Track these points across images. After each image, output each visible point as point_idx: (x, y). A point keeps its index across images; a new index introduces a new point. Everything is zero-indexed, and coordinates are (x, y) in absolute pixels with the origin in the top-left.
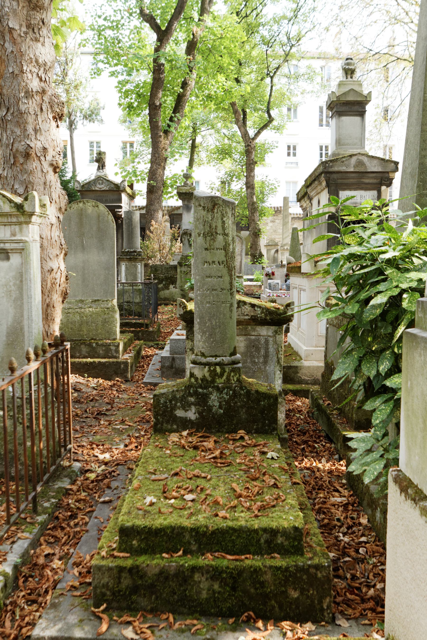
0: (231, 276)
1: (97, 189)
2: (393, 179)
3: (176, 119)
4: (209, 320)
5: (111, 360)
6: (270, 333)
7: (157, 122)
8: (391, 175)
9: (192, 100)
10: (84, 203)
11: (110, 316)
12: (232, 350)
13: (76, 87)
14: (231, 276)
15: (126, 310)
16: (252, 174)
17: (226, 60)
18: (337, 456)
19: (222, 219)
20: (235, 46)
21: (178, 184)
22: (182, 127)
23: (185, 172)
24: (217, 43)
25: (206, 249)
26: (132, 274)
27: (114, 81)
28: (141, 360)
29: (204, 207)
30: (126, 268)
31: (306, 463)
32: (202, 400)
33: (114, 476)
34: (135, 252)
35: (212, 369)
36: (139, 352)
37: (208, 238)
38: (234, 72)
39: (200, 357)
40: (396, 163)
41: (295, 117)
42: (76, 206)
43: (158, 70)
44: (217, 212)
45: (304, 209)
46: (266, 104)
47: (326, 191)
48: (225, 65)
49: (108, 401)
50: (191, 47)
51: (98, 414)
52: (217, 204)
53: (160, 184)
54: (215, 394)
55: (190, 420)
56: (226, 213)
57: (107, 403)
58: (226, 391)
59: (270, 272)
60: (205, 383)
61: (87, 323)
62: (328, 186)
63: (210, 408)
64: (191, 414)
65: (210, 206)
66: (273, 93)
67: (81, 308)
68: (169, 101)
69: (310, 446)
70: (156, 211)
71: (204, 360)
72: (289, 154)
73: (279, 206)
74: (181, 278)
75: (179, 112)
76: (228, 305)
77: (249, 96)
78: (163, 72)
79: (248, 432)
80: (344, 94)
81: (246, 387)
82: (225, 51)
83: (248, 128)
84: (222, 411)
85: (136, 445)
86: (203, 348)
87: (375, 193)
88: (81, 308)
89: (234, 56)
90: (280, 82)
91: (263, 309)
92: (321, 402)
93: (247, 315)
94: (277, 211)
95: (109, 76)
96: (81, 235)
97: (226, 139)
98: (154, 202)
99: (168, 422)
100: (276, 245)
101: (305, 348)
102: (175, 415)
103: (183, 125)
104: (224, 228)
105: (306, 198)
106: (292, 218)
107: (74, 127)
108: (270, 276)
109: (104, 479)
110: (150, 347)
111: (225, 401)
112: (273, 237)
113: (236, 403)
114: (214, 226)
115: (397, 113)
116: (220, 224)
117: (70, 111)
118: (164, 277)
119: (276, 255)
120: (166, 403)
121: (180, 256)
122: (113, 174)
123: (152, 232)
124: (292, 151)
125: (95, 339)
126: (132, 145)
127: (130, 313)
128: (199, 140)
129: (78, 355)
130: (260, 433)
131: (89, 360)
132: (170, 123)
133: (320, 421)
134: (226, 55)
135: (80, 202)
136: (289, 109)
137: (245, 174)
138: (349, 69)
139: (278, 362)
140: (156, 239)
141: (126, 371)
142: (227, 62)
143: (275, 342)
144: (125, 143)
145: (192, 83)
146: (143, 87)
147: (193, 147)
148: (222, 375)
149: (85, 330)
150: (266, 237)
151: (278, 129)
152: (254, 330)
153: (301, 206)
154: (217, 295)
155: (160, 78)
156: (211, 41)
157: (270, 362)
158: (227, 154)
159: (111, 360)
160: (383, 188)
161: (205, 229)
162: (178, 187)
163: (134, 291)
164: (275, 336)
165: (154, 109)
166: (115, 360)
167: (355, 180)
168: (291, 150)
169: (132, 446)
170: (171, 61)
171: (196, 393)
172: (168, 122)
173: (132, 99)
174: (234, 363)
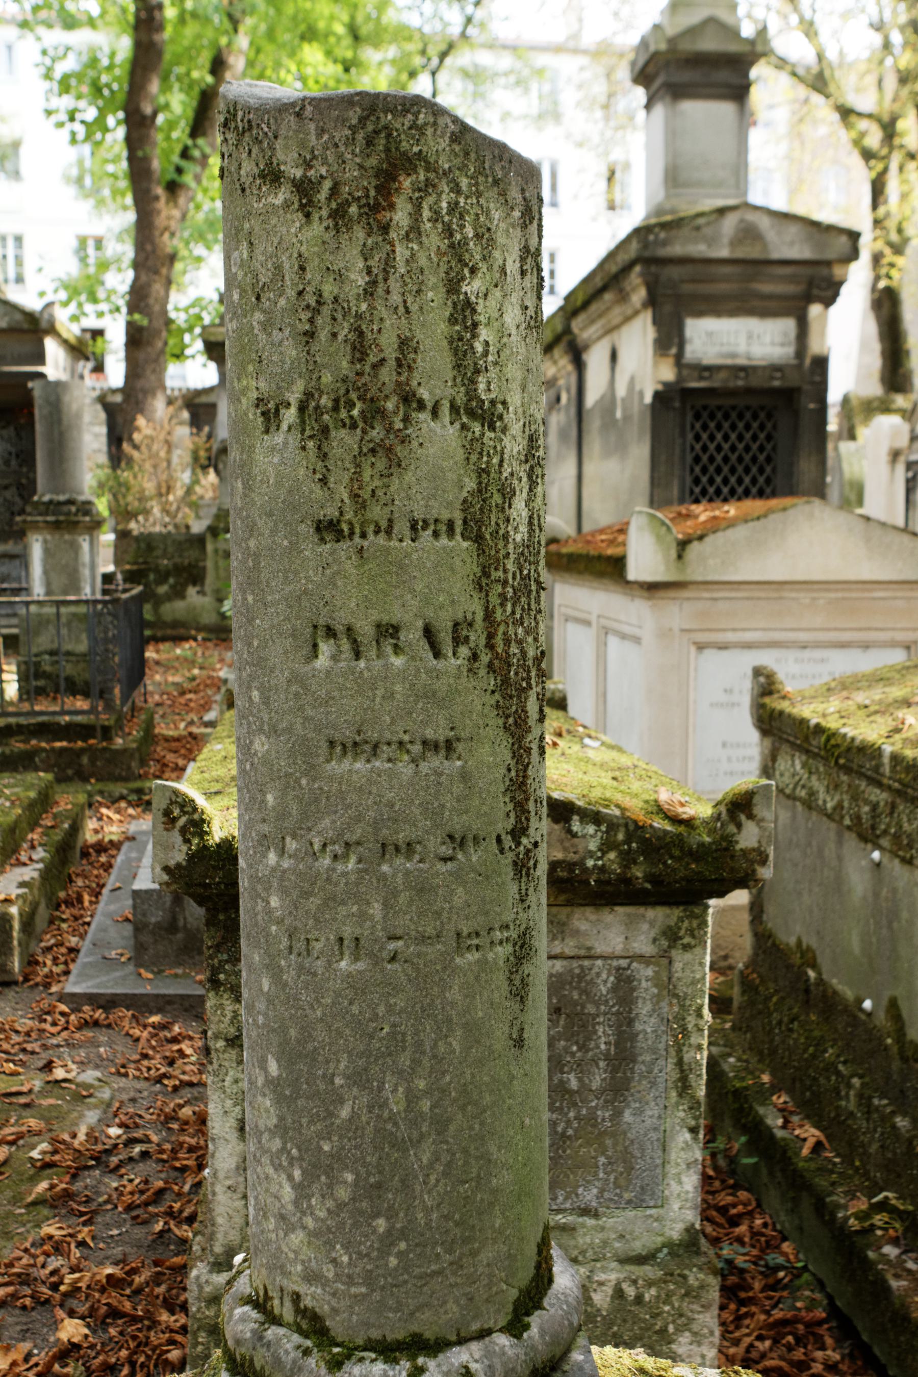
2: (840, 284)
3: (196, 153)
4: (358, 1078)
6: (643, 944)
7: (146, 160)
8: (837, 271)
19: (453, 286)
21: (207, 320)
25: (329, 529)
26: (65, 571)
30: (48, 552)
34: (71, 502)
37: (344, 442)
40: (854, 236)
44: (414, 232)
47: (647, 317)
52: (408, 163)
53: (158, 323)
56: (485, 236)
62: (652, 301)
65: (355, 175)
70: (150, 392)
74: (217, 567)
75: (204, 134)
76: (504, 951)
78: (160, 28)
86: (311, 1277)
87: (788, 325)
91: (612, 826)
110: (113, 801)
114: (388, 343)
116: (433, 329)
121: (214, 510)
123: (136, 447)
126: (99, 243)
132: (183, 163)
133: (773, 1198)
139: (684, 1086)
140: (148, 466)
143: (667, 987)
144: (82, 242)
145: (237, 63)
154: (422, 889)
157: (639, 1085)
160: (815, 310)
161: (313, 368)
164: (665, 956)
165: (139, 126)
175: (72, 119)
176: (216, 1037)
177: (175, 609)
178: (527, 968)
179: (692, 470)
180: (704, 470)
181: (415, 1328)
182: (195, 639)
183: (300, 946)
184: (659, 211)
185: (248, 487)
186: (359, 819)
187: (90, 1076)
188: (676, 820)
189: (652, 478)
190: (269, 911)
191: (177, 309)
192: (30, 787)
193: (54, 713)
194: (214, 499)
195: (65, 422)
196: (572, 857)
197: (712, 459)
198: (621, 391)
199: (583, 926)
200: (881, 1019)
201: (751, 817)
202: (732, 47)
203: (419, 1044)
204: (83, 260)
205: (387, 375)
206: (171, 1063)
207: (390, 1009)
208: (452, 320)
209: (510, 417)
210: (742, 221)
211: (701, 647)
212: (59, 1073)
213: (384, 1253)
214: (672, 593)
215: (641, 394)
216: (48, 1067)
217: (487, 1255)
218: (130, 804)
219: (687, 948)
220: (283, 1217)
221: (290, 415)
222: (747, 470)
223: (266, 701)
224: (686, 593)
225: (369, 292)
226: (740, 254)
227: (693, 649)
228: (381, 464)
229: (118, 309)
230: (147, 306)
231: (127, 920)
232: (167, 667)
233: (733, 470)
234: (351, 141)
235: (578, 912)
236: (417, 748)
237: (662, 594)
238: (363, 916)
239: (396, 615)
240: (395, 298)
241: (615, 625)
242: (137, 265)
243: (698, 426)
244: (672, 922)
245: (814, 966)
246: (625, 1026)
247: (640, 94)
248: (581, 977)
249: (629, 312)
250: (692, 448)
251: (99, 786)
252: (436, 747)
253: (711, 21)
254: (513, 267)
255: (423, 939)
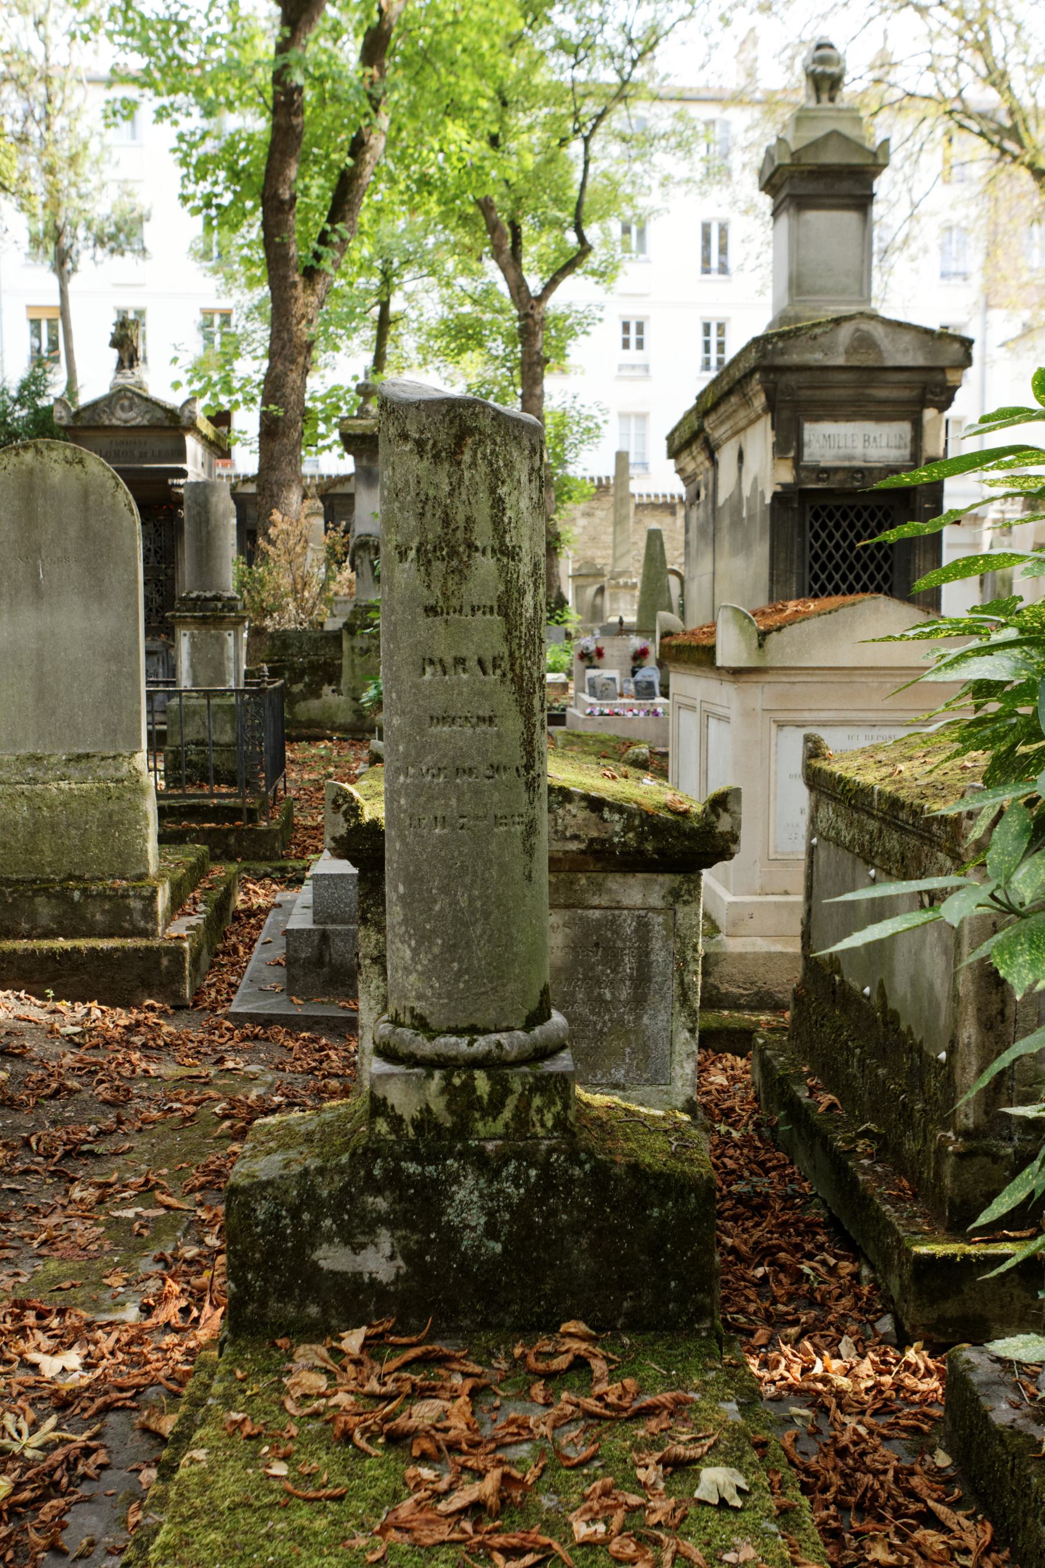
0: (528, 713)
1: (115, 422)
2: (955, 388)
3: (335, 239)
4: (444, 890)
5: (130, 943)
7: (284, 246)
8: (951, 377)
9: (376, 195)
10: (38, 452)
11: (125, 805)
12: (533, 1004)
13: (73, 160)
14: (528, 713)
15: (190, 764)
16: (538, 391)
17: (468, 84)
18: (886, 1325)
19: (493, 490)
20: (493, 46)
21: (344, 413)
22: (353, 262)
23: (361, 380)
24: (445, 36)
25: (431, 610)
26: (209, 662)
27: (166, 134)
28: (230, 926)
29: (420, 444)
30: (193, 645)
31: (788, 1368)
32: (420, 1208)
33: (85, 1477)
35: (457, 1081)
36: (221, 907)
37: (439, 567)
38: (489, 118)
39: (407, 1033)
41: (642, 248)
42: (14, 459)
43: (285, 105)
44: (474, 464)
45: (688, 479)
46: (572, 208)
47: (766, 421)
48: (466, 98)
49: (107, 1095)
50: (375, 46)
51: (67, 1155)
52: (469, 431)
53: (294, 414)
54: (470, 1182)
55: (373, 1281)
56: (509, 465)
57: (105, 1102)
58: (511, 1168)
59: (592, 648)
60: (431, 1138)
61: (53, 827)
62: (771, 407)
63: (451, 1236)
64: (379, 1262)
65: (444, 438)
66: (589, 180)
67: (34, 781)
68: (314, 188)
69: (783, 1267)
71: (424, 1047)
72: (626, 344)
73: (603, 474)
74: (353, 665)
76: (519, 828)
77: (527, 186)
78: (300, 111)
79: (602, 1328)
80: (814, 145)
81: (591, 1154)
82: (466, 59)
83: (525, 274)
84: (498, 1248)
85: (183, 1303)
86: (420, 997)
87: (904, 428)
88: (34, 781)
89: (489, 72)
90: (608, 155)
92: (803, 1094)
93: (575, 837)
94: (602, 487)
95: (155, 122)
96: (32, 552)
97: (468, 301)
98: (279, 462)
99: (284, 1293)
100: (599, 574)
101: (729, 898)
102: (315, 1263)
103: (356, 255)
104: (499, 528)
105: (695, 448)
106: (638, 506)
107: (69, 266)
108: (591, 659)
109: (45, 1498)
110: (259, 878)
111: (508, 1207)
112: (589, 553)
113: (553, 1213)
114: (461, 519)
115: (899, 239)
116: (483, 511)
117: (60, 223)
118: (304, 662)
119: (598, 600)
120: (278, 1218)
121: (350, 607)
122: (164, 381)
123: (271, 542)
124: (633, 336)
125: (79, 879)
126: (226, 317)
127: (204, 774)
128: (396, 305)
129: (25, 926)
130: (648, 1328)
131: (62, 943)
132: (322, 249)
133: (800, 1154)
134: (469, 70)
135: (26, 447)
136: (626, 230)
137: (520, 391)
138: (824, 76)
139: (684, 998)
141: (175, 975)
142: (471, 88)
143: (673, 930)
144: (208, 314)
145: (377, 143)
146: (246, 152)
147: (384, 323)
148: (495, 1106)
149: (45, 848)
150: (571, 553)
151: (601, 275)
152: (599, 888)
153: (680, 471)
154: (477, 792)
155: (291, 128)
156: (428, 32)
157: (653, 998)
158: (470, 337)
159: (130, 943)
160: (929, 414)
161: (424, 531)
162: (343, 419)
163: (212, 713)
164: (671, 908)
165: (276, 211)
166: (141, 943)
167: (850, 392)
168: (634, 333)
169: (170, 1312)
170: (321, 79)
171: (395, 1180)
172: (314, 245)
173: (215, 183)
174: (544, 1052)
175: (208, 205)
176: (365, 957)
177: (309, 708)
178: (533, 840)
179: (811, 568)
180: (823, 568)
181: (473, 1021)
182: (331, 740)
183: (415, 822)
184: (782, 318)
185: (391, 590)
186: (445, 756)
187: (254, 1068)
188: (675, 812)
189: (771, 574)
190: (400, 807)
191: (313, 398)
192: (191, 854)
193: (204, 796)
194: (351, 595)
195: (213, 522)
196: (604, 835)
197: (830, 557)
198: (746, 491)
199: (614, 887)
200: (875, 1000)
201: (726, 810)
202: (856, 160)
203: (475, 872)
204: (209, 338)
205: (460, 535)
206: (321, 1062)
207: (461, 853)
208: (492, 507)
209: (523, 554)
210: (857, 330)
211: (781, 725)
212: (230, 1065)
213: (457, 981)
214: (754, 678)
215: (762, 493)
216: (221, 1060)
217: (511, 987)
218: (274, 881)
219: (686, 903)
220: (405, 968)
221: (412, 554)
222: (865, 568)
223: (399, 698)
224: (767, 678)
225: (451, 494)
226: (855, 363)
227: (774, 727)
228: (457, 578)
229: (253, 400)
230: (283, 395)
231: (279, 964)
232: (303, 765)
233: (851, 568)
234: (443, 421)
235: (611, 876)
236: (474, 720)
237: (745, 678)
238: (447, 805)
239: (464, 653)
240: (464, 497)
241: (713, 709)
242: (272, 354)
243: (817, 525)
244: (676, 884)
245: (839, 972)
246: (643, 955)
247: (766, 202)
248: (613, 922)
249: (753, 416)
250: (812, 547)
251: (245, 865)
252: (484, 720)
253: (834, 134)
254: (524, 479)
255: (477, 818)
